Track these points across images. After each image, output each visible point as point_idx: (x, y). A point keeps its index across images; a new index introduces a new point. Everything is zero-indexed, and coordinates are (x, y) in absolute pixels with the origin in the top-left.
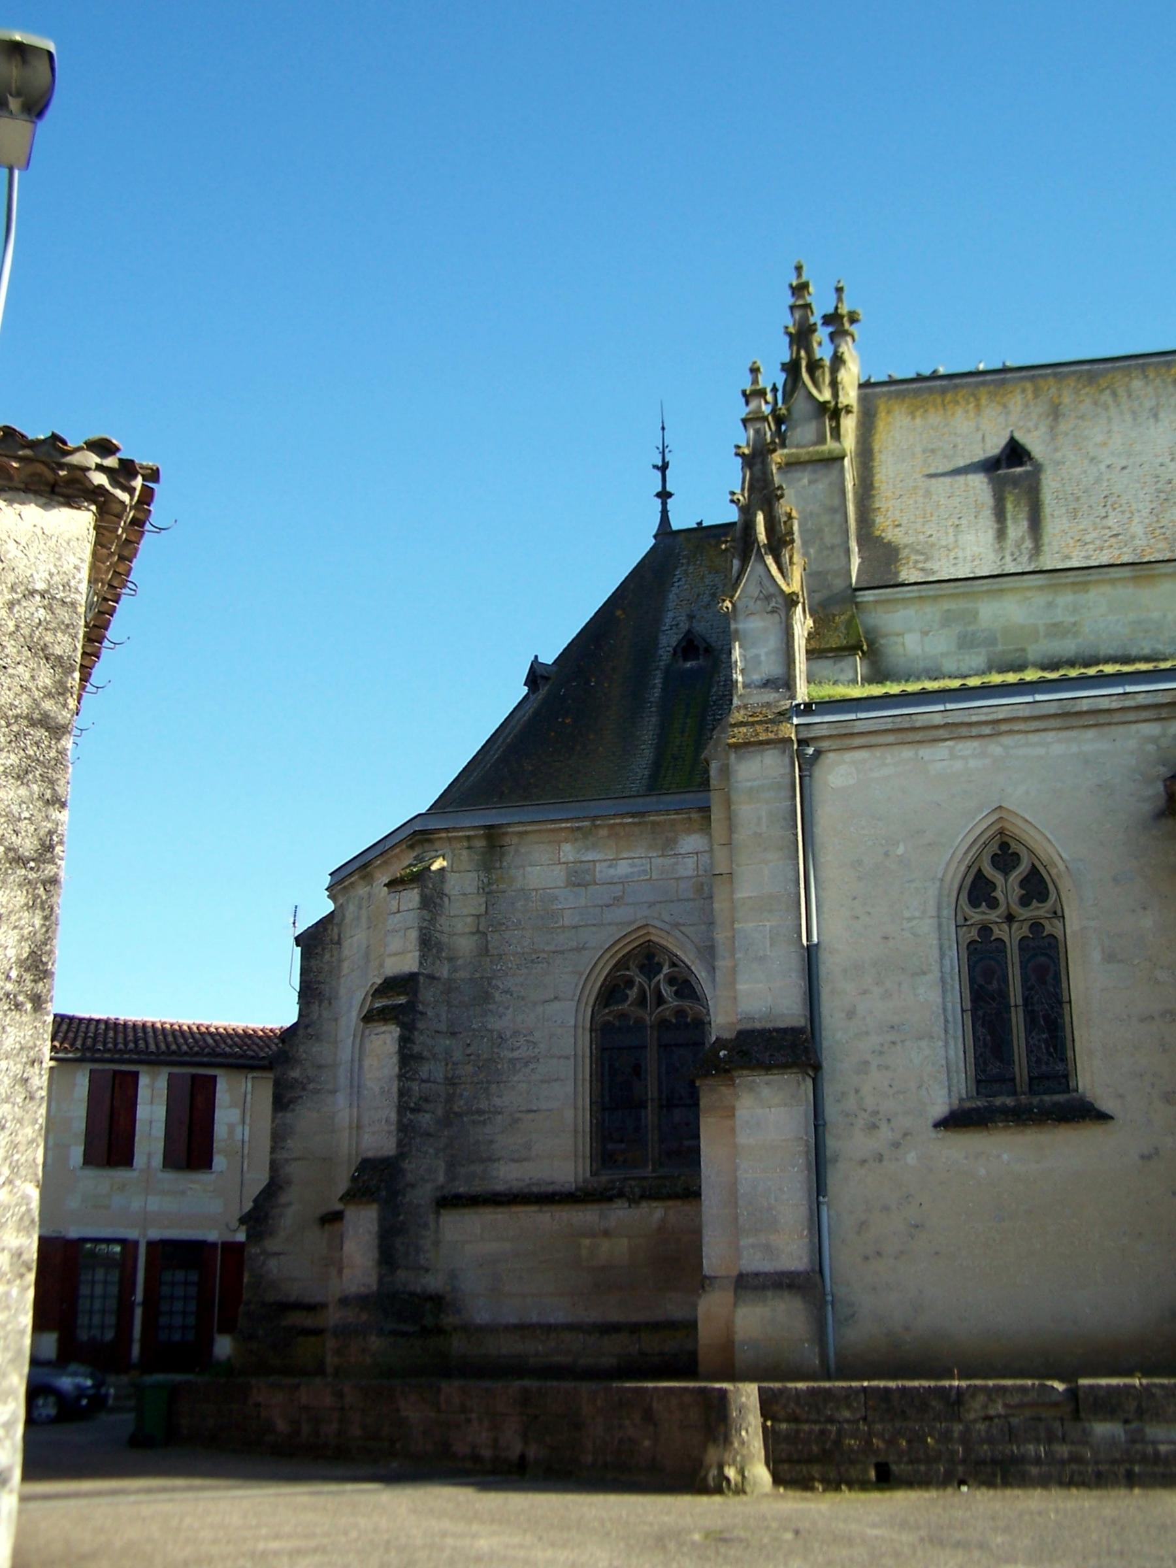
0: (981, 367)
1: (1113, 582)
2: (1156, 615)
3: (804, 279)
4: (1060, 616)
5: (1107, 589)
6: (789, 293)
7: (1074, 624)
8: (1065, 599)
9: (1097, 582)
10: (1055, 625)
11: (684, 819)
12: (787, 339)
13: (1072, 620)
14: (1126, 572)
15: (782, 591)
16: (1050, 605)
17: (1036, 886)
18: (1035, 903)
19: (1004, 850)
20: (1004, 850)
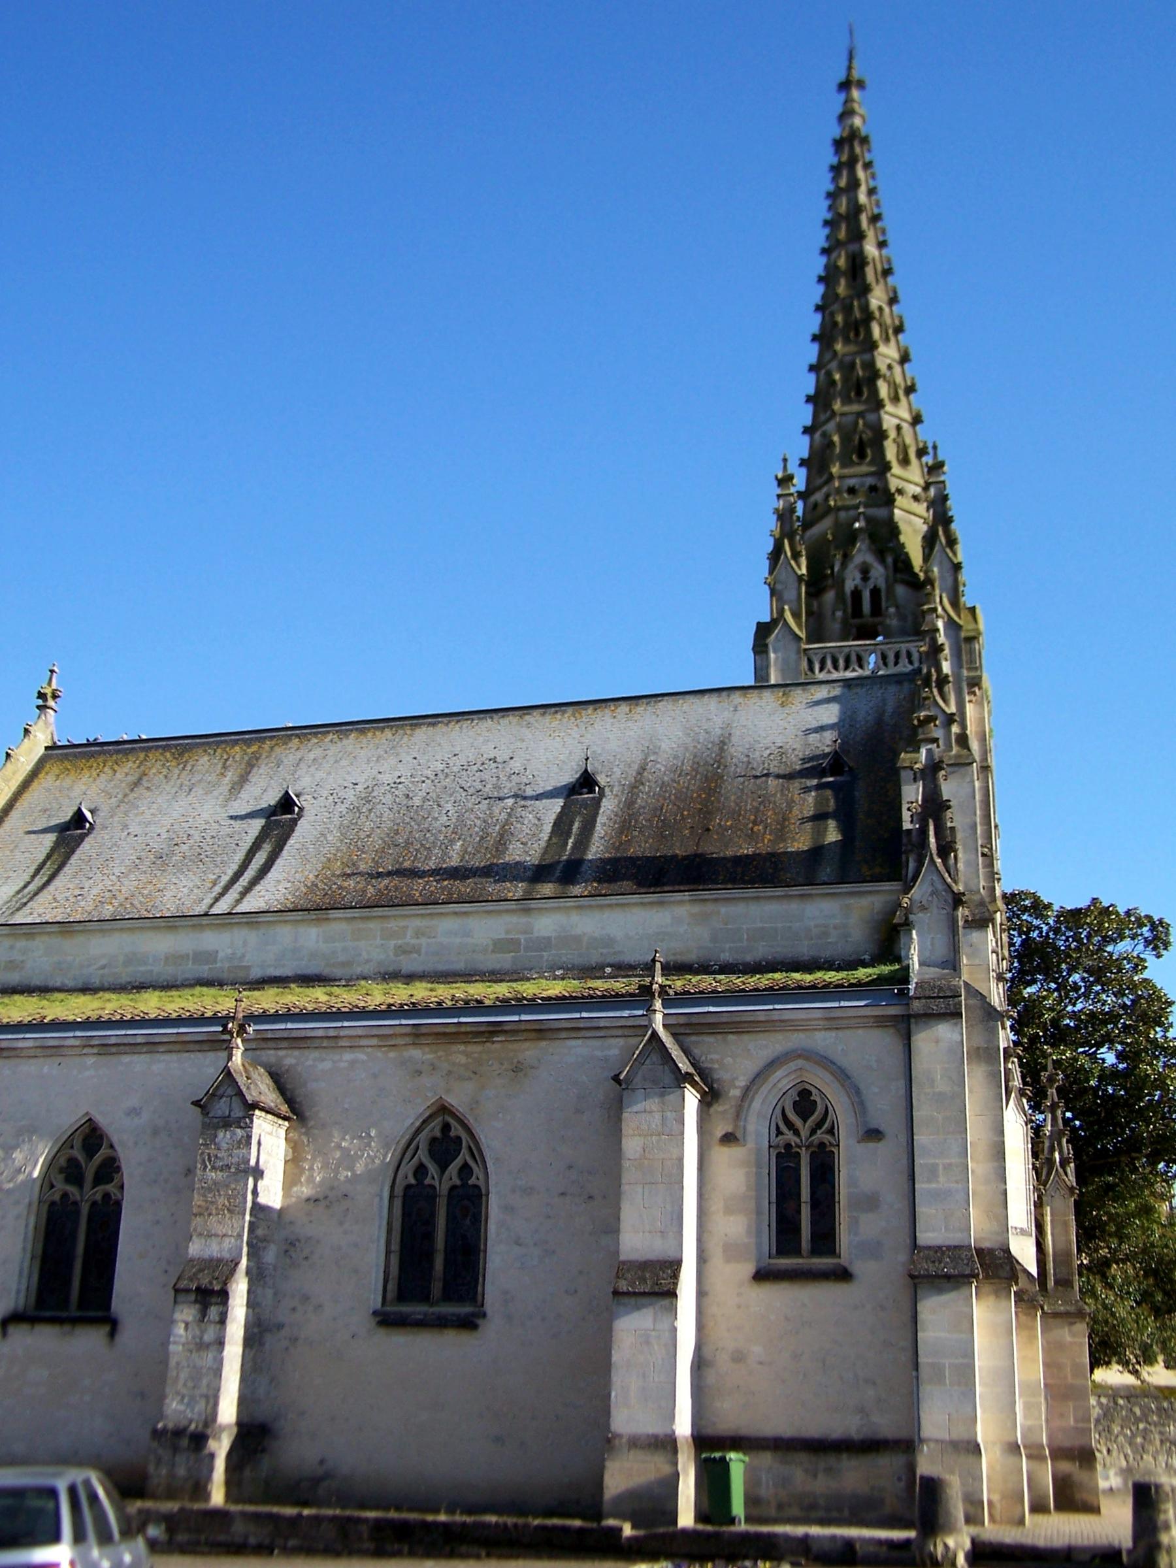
0: (126, 737)
1: (49, 933)
2: (70, 958)
3: (940, 458)
4: (16, 956)
5: (45, 938)
6: (776, 483)
7: (22, 962)
8: (21, 944)
9: (40, 933)
10: (11, 962)
11: (881, 980)
12: (775, 517)
13: (21, 958)
14: (55, 928)
15: (944, 711)
16: (12, 947)
17: (110, 1170)
18: (438, 1134)
19: (91, 1136)
20: (91, 1136)
